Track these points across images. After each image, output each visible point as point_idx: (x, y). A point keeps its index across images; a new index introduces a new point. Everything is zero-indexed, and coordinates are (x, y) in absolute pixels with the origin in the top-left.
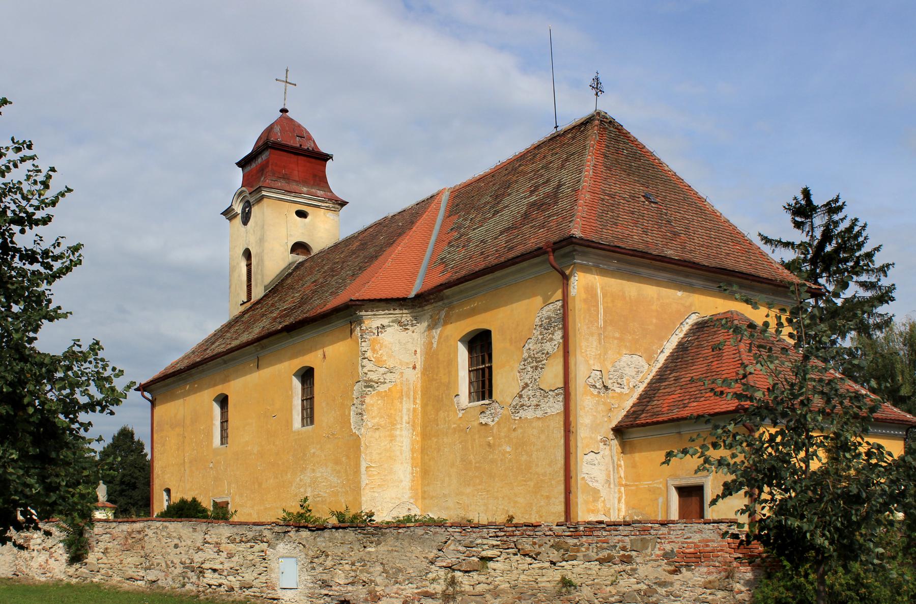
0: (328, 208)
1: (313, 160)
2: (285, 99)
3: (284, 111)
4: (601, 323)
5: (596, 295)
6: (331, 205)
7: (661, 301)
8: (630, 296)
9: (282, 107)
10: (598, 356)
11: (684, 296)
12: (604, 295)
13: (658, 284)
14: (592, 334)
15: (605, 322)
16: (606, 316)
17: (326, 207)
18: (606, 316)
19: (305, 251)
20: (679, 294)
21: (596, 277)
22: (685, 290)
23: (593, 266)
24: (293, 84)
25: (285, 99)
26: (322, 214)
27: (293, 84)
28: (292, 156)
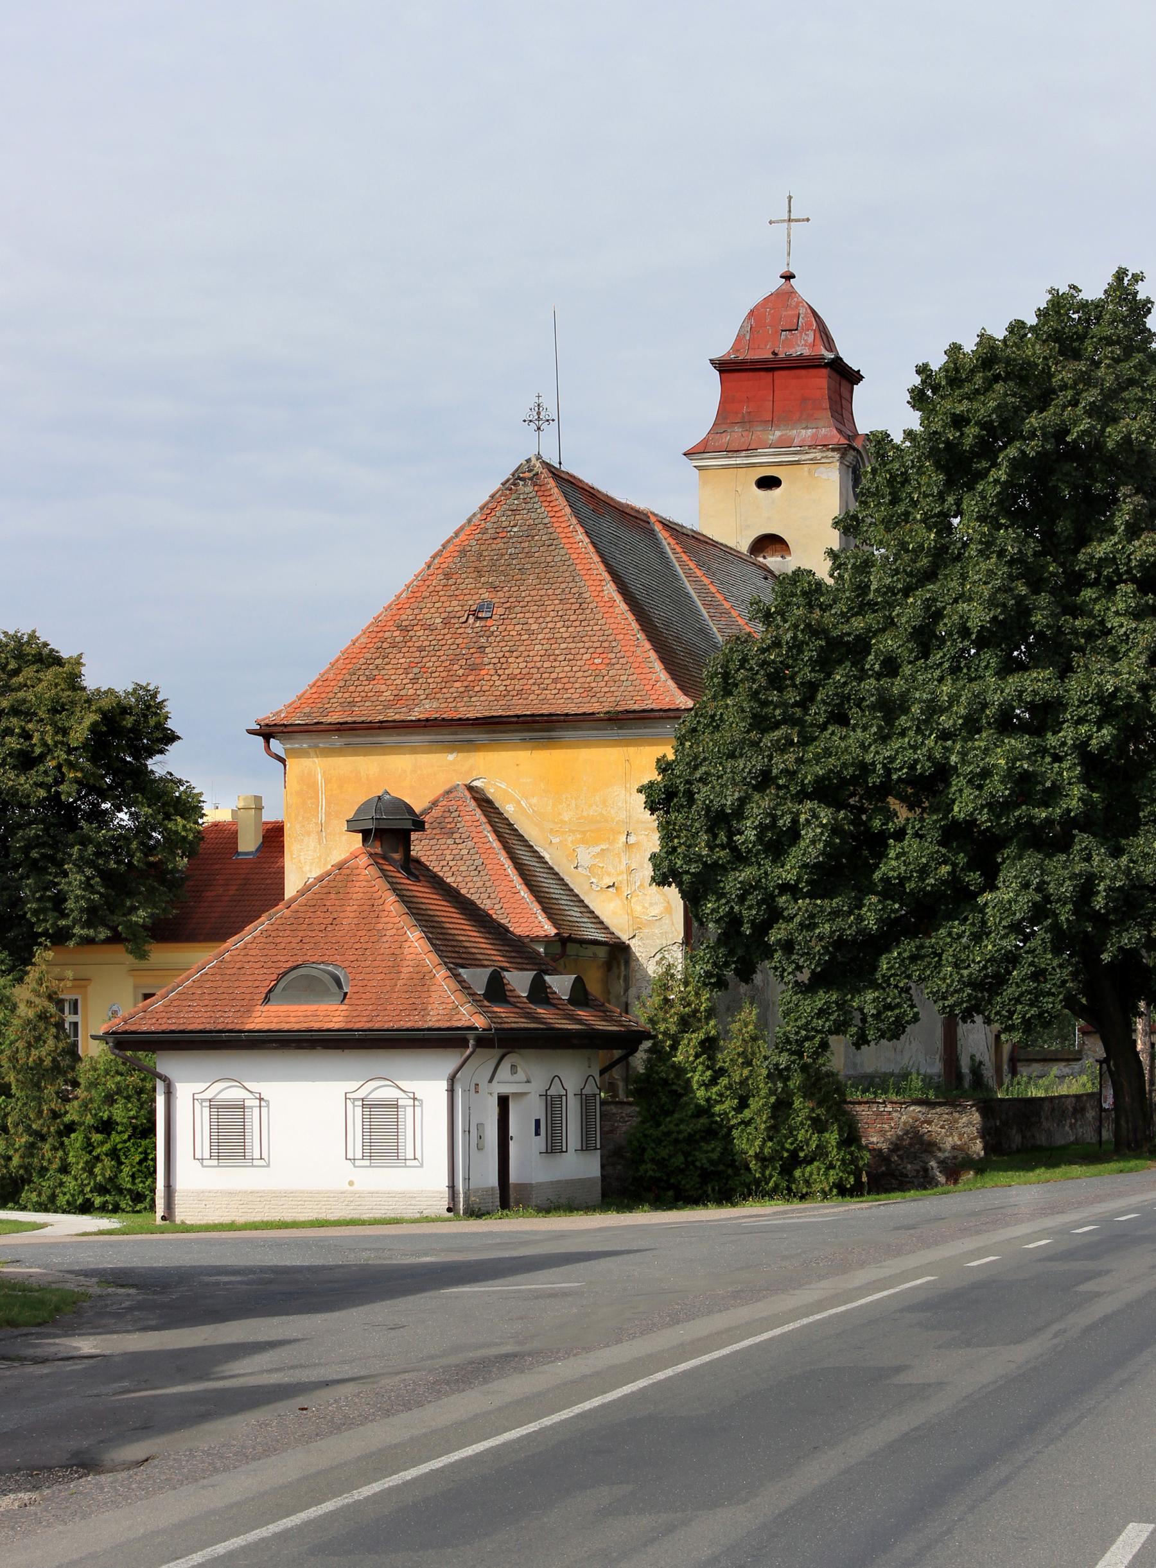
0: (815, 462)
1: (803, 372)
2: (789, 254)
3: (788, 277)
4: (322, 816)
5: (315, 783)
6: (819, 455)
7: (419, 772)
8: (368, 775)
9: (783, 270)
10: (317, 860)
11: (459, 758)
12: (327, 781)
13: (414, 751)
14: (309, 834)
15: (328, 815)
16: (330, 807)
17: (812, 460)
18: (330, 807)
19: (778, 546)
20: (451, 757)
21: (316, 760)
22: (460, 751)
23: (310, 747)
24: (803, 220)
25: (789, 254)
26: (806, 474)
27: (803, 220)
28: (762, 374)
